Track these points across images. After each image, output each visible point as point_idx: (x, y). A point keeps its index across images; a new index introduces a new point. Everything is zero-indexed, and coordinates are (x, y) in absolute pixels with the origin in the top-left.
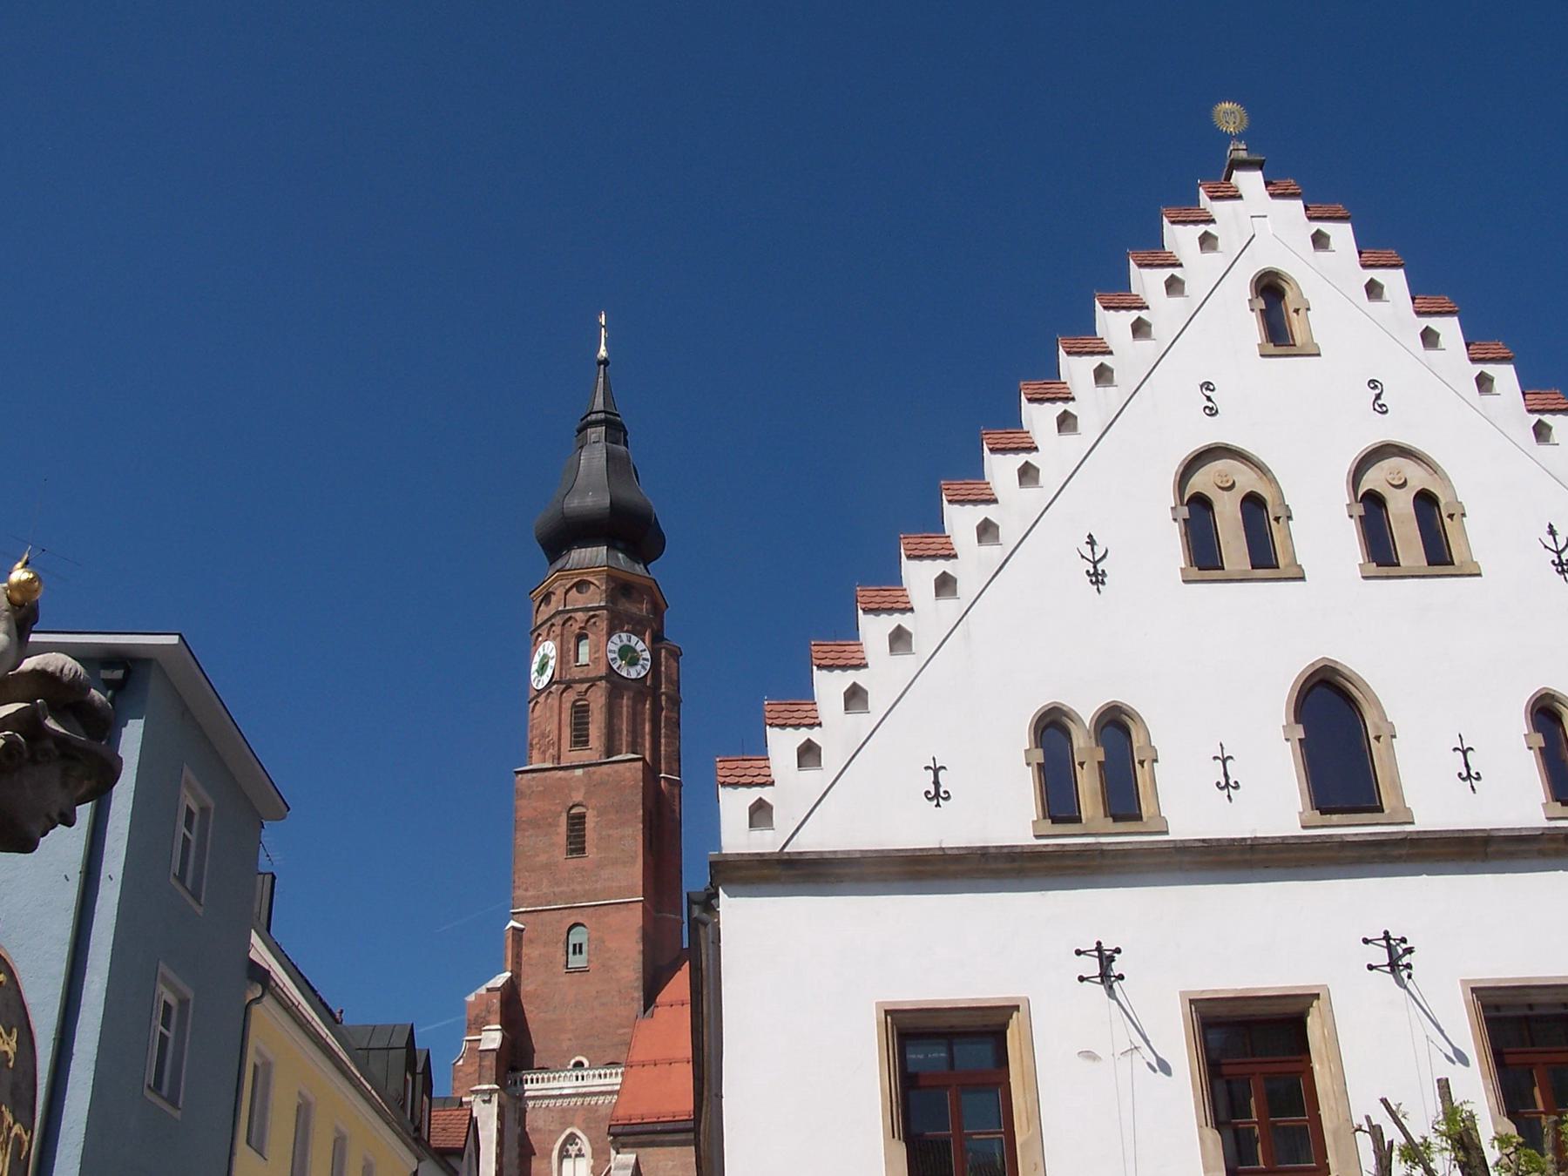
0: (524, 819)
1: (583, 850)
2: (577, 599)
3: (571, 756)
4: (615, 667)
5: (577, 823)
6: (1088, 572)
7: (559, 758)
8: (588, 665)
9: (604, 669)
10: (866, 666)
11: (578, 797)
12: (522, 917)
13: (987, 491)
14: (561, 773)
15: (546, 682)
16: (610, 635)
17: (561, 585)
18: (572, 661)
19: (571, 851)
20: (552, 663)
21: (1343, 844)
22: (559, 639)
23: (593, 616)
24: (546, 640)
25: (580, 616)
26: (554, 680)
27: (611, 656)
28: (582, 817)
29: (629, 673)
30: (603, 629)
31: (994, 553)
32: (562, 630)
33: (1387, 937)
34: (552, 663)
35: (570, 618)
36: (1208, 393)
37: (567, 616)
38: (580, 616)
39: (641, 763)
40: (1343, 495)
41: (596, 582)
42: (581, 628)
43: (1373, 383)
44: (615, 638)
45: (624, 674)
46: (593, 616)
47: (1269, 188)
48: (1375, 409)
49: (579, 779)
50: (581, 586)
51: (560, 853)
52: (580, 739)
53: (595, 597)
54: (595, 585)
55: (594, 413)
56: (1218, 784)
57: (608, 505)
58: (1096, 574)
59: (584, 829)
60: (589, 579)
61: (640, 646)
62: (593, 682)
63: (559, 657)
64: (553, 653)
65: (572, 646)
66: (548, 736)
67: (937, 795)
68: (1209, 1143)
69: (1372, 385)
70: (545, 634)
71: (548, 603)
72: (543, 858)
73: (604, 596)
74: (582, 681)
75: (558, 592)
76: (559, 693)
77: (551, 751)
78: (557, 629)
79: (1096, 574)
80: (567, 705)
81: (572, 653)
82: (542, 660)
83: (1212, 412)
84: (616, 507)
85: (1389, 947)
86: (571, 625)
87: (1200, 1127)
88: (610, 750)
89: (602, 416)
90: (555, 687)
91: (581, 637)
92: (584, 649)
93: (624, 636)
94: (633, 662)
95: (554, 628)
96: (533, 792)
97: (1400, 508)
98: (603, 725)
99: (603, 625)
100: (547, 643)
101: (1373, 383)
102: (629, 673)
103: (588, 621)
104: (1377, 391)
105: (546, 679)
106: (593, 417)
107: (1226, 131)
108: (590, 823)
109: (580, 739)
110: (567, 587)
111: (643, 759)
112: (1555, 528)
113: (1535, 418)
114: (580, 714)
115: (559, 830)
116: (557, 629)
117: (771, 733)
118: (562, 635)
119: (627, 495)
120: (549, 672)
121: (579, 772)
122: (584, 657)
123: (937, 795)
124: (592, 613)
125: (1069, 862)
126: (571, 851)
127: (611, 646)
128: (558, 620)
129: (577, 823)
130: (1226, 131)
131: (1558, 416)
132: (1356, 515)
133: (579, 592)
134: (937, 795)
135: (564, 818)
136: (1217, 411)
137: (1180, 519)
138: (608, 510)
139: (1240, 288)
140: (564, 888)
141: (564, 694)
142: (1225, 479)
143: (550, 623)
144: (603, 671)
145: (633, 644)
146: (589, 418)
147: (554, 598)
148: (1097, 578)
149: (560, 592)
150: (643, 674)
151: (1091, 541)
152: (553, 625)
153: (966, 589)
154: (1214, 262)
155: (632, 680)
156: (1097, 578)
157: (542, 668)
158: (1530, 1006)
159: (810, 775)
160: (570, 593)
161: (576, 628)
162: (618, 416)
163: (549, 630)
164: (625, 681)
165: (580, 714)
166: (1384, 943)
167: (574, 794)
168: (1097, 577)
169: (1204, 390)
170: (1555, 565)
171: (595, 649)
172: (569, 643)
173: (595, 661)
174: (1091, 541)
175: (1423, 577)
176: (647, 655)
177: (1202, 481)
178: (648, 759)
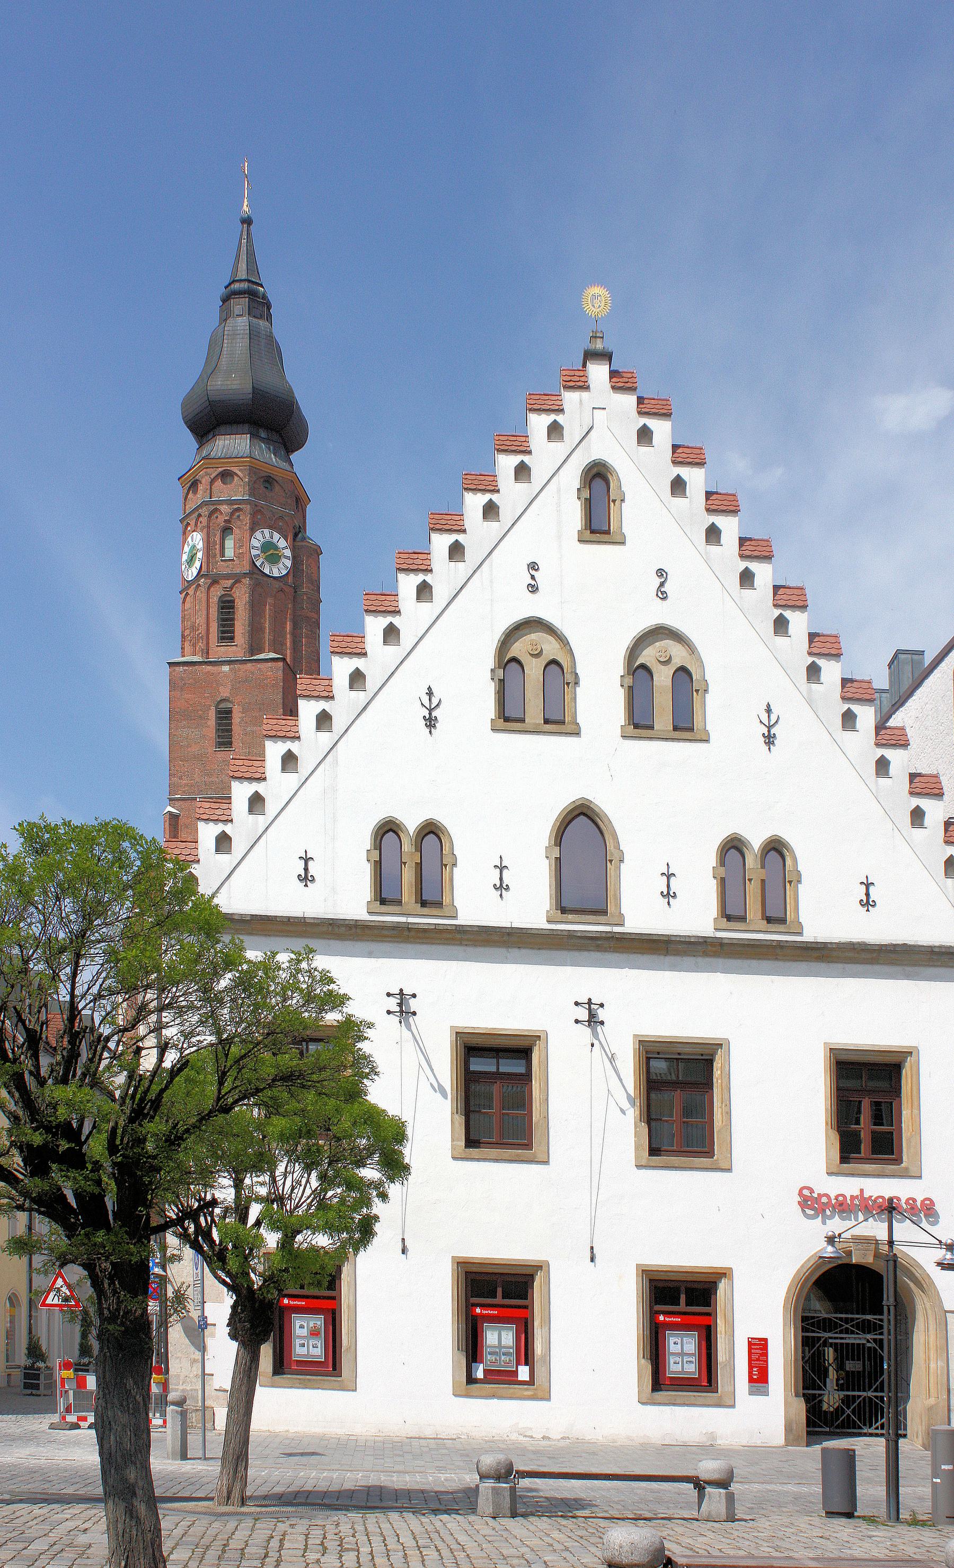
0: (178, 710)
1: (230, 743)
2: (223, 491)
3: (220, 651)
4: (258, 564)
5: (224, 716)
6: (424, 717)
7: (208, 653)
8: (233, 560)
9: (248, 566)
10: (265, 779)
11: (225, 692)
12: (178, 804)
13: (359, 645)
14: (209, 668)
15: (195, 574)
16: (253, 530)
17: (207, 474)
18: (218, 555)
19: (220, 744)
20: (200, 555)
21: (571, 935)
22: (205, 530)
23: (238, 510)
24: (194, 531)
25: (225, 508)
26: (202, 573)
27: (254, 552)
28: (229, 712)
29: (271, 570)
30: (246, 524)
31: (360, 697)
32: (209, 522)
33: (590, 1002)
34: (200, 555)
35: (216, 510)
36: (533, 572)
37: (212, 508)
38: (225, 508)
39: (281, 664)
40: (619, 668)
41: (239, 473)
42: (225, 521)
43: (661, 573)
44: (258, 534)
45: (267, 571)
46: (238, 510)
47: (613, 380)
48: (657, 595)
49: (226, 675)
50: (226, 476)
51: (209, 745)
52: (227, 635)
53: (237, 491)
54: (239, 477)
55: (238, 281)
56: (495, 885)
57: (250, 390)
58: (430, 719)
59: (231, 724)
60: (235, 470)
61: (282, 543)
62: (237, 578)
63: (205, 550)
64: (200, 545)
65: (217, 539)
66: (198, 630)
67: (306, 877)
68: (457, 1124)
69: (659, 574)
70: (193, 523)
71: (195, 492)
72: (195, 749)
73: (247, 488)
74: (227, 577)
75: (203, 481)
76: (207, 586)
77: (200, 644)
78: (204, 520)
79: (430, 719)
80: (214, 600)
81: (218, 547)
82: (191, 551)
83: (533, 589)
84: (257, 392)
85: (590, 1009)
86: (217, 517)
87: (452, 1113)
88: (254, 647)
89: (245, 285)
90: (203, 580)
91: (226, 530)
92: (229, 543)
93: (266, 531)
94: (274, 559)
95: (201, 519)
96: (185, 684)
97: (663, 677)
98: (247, 622)
99: (247, 520)
100: (195, 533)
101: (661, 573)
102: (271, 570)
103: (232, 514)
104: (663, 580)
105: (194, 571)
106: (236, 286)
107: (607, 291)
108: (237, 717)
109: (227, 635)
110: (212, 476)
111: (284, 660)
112: (772, 707)
113: (777, 612)
114: (227, 606)
115: (209, 723)
116: (204, 520)
117: (201, 825)
118: (209, 527)
119: (269, 381)
120: (197, 564)
121: (226, 668)
122: (229, 553)
123: (306, 877)
124: (236, 506)
125: (386, 932)
126: (220, 744)
127: (255, 543)
128: (204, 511)
129: (224, 716)
130: (607, 291)
131: (797, 612)
132: (626, 686)
133: (224, 483)
134: (306, 878)
135: (212, 714)
136: (537, 588)
137: (496, 679)
138: (251, 396)
139: (572, 477)
140: (214, 779)
141: (212, 589)
142: (535, 647)
143: (196, 514)
144: (246, 568)
145: (275, 540)
146: (232, 286)
147: (201, 487)
148: (431, 722)
149: (205, 481)
150: (284, 572)
151: (430, 693)
152: (200, 515)
153: (339, 723)
154: (559, 449)
155: (275, 578)
156: (431, 722)
157: (192, 559)
158: (679, 1054)
159: (223, 858)
160: (216, 484)
161: (221, 520)
162: (262, 286)
163: (197, 520)
164: (266, 579)
165: (227, 606)
166: (587, 1006)
167: (221, 689)
168: (430, 722)
169: (530, 570)
170: (764, 737)
171: (239, 544)
172: (215, 535)
173: (239, 556)
174: (430, 693)
175: (666, 739)
176: (288, 553)
177: (518, 649)
178: (288, 660)
